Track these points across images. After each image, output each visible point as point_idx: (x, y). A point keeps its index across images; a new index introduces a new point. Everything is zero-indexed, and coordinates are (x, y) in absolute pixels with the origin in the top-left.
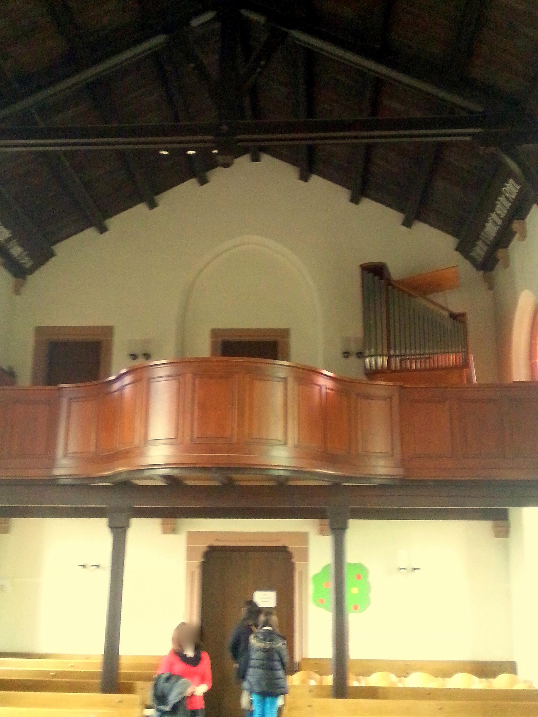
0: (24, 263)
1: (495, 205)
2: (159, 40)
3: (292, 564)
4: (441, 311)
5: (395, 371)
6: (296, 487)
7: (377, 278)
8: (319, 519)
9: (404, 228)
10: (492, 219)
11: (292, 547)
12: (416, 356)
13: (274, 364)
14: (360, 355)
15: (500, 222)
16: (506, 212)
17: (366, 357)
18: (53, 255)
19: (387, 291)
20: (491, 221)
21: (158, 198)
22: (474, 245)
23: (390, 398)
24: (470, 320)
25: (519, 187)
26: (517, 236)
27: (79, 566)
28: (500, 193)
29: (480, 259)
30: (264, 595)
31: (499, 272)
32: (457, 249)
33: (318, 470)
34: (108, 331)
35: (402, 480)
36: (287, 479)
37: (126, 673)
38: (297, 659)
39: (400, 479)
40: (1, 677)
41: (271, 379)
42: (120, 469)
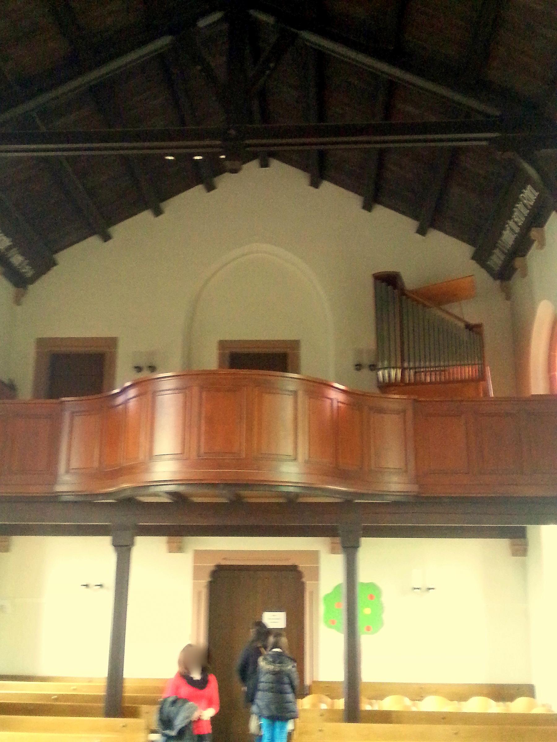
0: (25, 273)
1: (512, 213)
2: (165, 41)
3: (303, 584)
4: (456, 322)
5: (409, 384)
6: (306, 504)
7: (390, 288)
8: (330, 538)
9: (418, 236)
10: (509, 226)
11: (302, 566)
12: (431, 369)
13: (284, 377)
14: (373, 367)
15: (517, 230)
16: (523, 219)
17: (379, 369)
18: (55, 264)
19: (401, 301)
20: (508, 228)
21: (163, 205)
22: (491, 254)
23: (404, 411)
24: (487, 331)
25: (537, 194)
26: (535, 244)
27: (82, 585)
28: (518, 200)
29: (497, 269)
30: (274, 616)
31: (517, 282)
32: (473, 258)
33: (329, 487)
34: (112, 342)
35: (416, 497)
36: (297, 495)
37: (130, 697)
38: (308, 682)
39: (414, 496)
40: (1, 700)
41: (280, 392)
42: (125, 485)
